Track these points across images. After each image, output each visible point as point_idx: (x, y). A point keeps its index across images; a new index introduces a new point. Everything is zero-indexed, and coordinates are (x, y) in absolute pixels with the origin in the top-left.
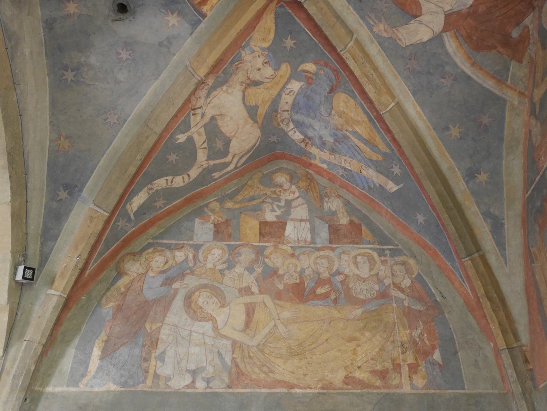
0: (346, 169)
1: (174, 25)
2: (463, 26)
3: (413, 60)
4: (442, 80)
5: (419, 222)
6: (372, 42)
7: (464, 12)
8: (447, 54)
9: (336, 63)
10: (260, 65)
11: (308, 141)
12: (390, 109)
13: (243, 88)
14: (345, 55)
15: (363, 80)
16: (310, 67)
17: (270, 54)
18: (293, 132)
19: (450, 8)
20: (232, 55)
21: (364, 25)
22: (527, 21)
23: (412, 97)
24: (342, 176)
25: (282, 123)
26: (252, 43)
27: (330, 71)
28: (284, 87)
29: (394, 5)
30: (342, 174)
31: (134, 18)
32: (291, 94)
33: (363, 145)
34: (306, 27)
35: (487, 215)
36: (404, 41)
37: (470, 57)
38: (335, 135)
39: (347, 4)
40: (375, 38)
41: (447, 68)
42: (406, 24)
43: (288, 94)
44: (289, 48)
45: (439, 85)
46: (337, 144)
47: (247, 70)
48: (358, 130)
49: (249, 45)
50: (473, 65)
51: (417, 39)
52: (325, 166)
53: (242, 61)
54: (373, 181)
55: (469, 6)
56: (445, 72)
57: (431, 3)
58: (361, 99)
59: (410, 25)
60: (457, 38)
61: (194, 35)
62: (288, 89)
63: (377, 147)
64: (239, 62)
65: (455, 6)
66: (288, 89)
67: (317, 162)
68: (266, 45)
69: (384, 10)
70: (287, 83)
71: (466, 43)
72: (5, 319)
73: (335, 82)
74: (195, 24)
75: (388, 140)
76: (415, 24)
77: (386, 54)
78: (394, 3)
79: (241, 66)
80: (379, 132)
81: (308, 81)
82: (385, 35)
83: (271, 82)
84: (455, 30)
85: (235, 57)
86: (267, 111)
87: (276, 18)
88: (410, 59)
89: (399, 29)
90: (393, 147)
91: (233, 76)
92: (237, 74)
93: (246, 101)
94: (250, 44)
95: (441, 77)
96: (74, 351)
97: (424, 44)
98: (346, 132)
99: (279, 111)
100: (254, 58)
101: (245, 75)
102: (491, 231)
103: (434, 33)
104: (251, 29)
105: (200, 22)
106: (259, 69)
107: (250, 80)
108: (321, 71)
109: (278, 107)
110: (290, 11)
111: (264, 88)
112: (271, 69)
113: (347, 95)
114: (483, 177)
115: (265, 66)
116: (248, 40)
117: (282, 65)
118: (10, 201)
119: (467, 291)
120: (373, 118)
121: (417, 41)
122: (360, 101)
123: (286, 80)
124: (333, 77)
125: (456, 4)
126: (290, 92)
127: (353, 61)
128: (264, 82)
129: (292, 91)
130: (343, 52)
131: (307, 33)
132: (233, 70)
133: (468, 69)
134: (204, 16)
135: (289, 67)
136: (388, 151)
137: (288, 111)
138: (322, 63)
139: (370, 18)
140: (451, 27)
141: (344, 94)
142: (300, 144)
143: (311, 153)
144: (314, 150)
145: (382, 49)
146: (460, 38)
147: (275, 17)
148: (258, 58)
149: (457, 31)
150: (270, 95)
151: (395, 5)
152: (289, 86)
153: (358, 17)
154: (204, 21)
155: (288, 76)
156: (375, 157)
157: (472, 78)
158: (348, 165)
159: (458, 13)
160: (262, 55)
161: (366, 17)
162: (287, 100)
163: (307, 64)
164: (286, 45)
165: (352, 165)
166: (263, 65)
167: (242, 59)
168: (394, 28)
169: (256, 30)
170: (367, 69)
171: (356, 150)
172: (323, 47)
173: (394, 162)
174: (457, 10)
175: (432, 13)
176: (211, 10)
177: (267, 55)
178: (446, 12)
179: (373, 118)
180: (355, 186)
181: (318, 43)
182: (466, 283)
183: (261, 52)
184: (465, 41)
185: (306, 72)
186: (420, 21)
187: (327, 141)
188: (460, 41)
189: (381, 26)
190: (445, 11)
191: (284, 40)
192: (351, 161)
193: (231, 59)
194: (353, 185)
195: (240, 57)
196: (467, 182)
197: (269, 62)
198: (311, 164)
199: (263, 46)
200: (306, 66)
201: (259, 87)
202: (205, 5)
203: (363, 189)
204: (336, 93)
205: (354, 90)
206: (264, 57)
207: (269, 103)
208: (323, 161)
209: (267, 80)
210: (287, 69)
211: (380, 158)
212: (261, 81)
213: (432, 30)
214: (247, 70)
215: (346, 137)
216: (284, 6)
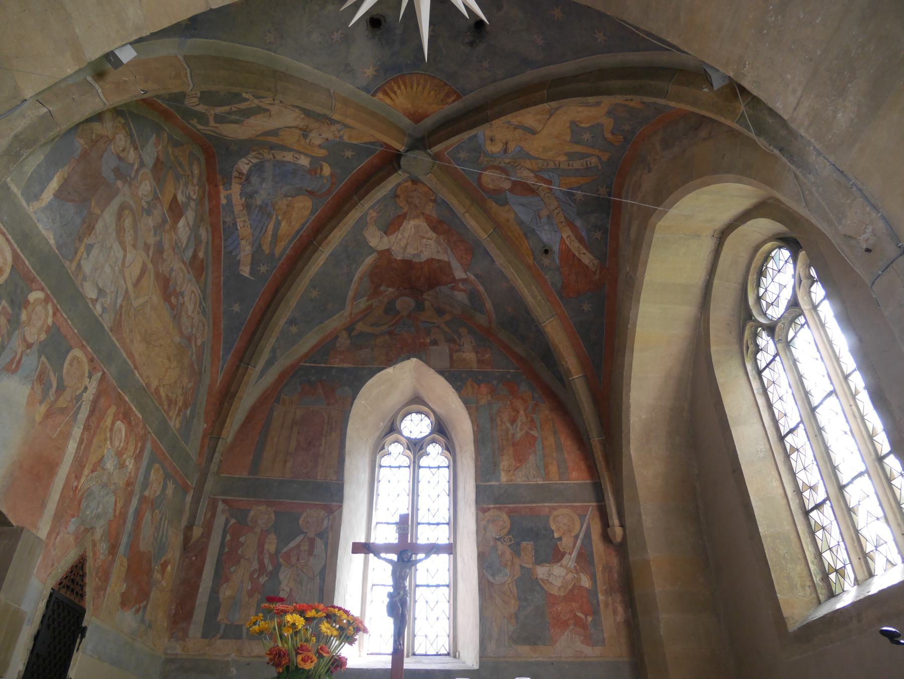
0: (235, 224)
1: (365, 73)
5: (232, 309)
8: (363, 261)
11: (244, 177)
16: (327, 170)
18: (248, 162)
22: (390, 290)
24: (225, 222)
25: (256, 154)
28: (301, 153)
30: (227, 221)
31: (370, 39)
32: (295, 159)
33: (271, 233)
35: (274, 351)
38: (267, 205)
42: (378, 229)
43: (293, 156)
44: (343, 154)
46: (258, 209)
48: (283, 224)
52: (224, 201)
54: (240, 253)
61: (356, 90)
62: (300, 156)
63: (276, 245)
66: (300, 156)
67: (223, 194)
70: (306, 155)
72: (69, 70)
74: (367, 90)
75: (287, 252)
80: (290, 242)
82: (369, 218)
89: (374, 226)
90: (283, 259)
96: (43, 157)
98: (275, 214)
99: (272, 151)
102: (266, 361)
105: (368, 91)
113: (311, 207)
114: (294, 329)
118: (211, 9)
119: (217, 380)
120: (301, 233)
126: (296, 158)
129: (298, 159)
133: (356, 278)
134: (374, 95)
135: (324, 155)
136: (277, 256)
137: (274, 158)
139: (379, 206)
141: (311, 203)
142: (234, 170)
143: (231, 185)
144: (236, 188)
148: (332, 134)
152: (302, 157)
153: (379, 198)
154: (369, 96)
155: (314, 155)
156: (266, 248)
158: (241, 225)
162: (288, 157)
163: (329, 168)
165: (244, 227)
171: (262, 229)
173: (269, 264)
176: (379, 99)
179: (301, 233)
180: (223, 238)
182: (222, 374)
183: (339, 135)
187: (256, 199)
189: (374, 214)
192: (247, 227)
194: (222, 236)
196: (286, 323)
198: (216, 186)
202: (383, 94)
203: (225, 247)
205: (319, 211)
208: (229, 198)
211: (267, 252)
215: (269, 216)
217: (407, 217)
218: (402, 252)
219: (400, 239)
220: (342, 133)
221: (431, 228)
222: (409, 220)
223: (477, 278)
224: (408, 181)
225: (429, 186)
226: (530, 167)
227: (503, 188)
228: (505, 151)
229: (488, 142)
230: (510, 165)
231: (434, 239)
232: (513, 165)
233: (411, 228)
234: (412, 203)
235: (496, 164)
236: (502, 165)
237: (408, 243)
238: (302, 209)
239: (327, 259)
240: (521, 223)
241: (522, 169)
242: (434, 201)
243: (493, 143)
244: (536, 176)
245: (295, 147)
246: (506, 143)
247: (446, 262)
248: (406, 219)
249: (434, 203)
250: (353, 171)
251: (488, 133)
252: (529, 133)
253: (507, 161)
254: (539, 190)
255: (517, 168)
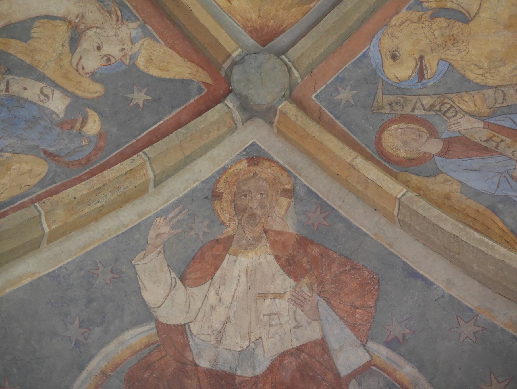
2: (166, 355)
3: (111, 275)
4: (77, 322)
6: (140, 216)
7: (188, 354)
8: (122, 330)
9: (102, 162)
10: (106, 50)
12: (40, 222)
13: (72, 17)
14: (138, 159)
15: (96, 182)
17: (124, 68)
19: (194, 332)
20: (135, 8)
21: (168, 204)
23: (47, 272)
26: (147, 41)
27: (86, 153)
28: (56, 86)
29: (202, 245)
32: (42, 97)
34: (164, 122)
36: (143, 262)
37: (116, 368)
39: (203, 179)
40: (147, 220)
41: (97, 331)
43: (42, 92)
44: (129, 96)
45: (69, 317)
47: (103, 29)
49: (145, 36)
50: (103, 373)
51: (146, 283)
53: (120, 21)
55: (197, 361)
56: (92, 328)
57: (203, 302)
58: (39, 193)
59: (168, 272)
60: (146, 347)
64: (120, 17)
65: (197, 340)
68: (141, 62)
69: (193, 233)
70: (65, 91)
71: (139, 361)
73: (67, 159)
76: (169, 280)
77: (120, 234)
78: (204, 245)
79: (112, 18)
81: (66, 123)
82: (152, 234)
83: (72, 65)
84: (159, 343)
85: (130, 11)
86: (12, 57)
87: (182, 81)
88: (112, 271)
89: (161, 256)
91: (98, 5)
92: (100, 11)
93: (45, 20)
94: (146, 39)
95: (83, 321)
97: (138, 292)
100: (122, 42)
101: (95, 24)
103: (155, 308)
104: (170, 42)
106: (99, 48)
107: (84, 32)
108: (86, 141)
109: (16, 75)
110: (192, 101)
111: (61, 54)
112: (96, 67)
115: (102, 58)
116: (154, 36)
117: (100, 85)
121: (142, 282)
122: (36, 192)
123: (71, 90)
124: (76, 158)
125: (201, 340)
126: (46, 96)
127: (129, 169)
128: (72, 55)
129: (48, 98)
130: (143, 156)
131: (154, 124)
132: (108, 5)
135: (96, 95)
137: (7, 90)
138: (102, 143)
140: (163, 336)
145: (129, 230)
146: (147, 350)
147: (184, 80)
148: (120, 47)
149: (158, 346)
150: (46, 64)
151: (201, 247)
152: (57, 94)
153: (181, 195)
155: (79, 93)
157: (80, 373)
159: (186, 346)
160: (125, 55)
161: (181, 206)
163: (98, 122)
164: (135, 92)
166: (106, 56)
167: (125, 22)
168: (163, 248)
169: (168, 49)
170: (109, 194)
172: (131, 146)
174: (190, 344)
175: (188, 303)
177: (124, 63)
178: (189, 326)
181: (137, 139)
183: (130, 53)
184: (143, 359)
185: (83, 121)
186: (174, 287)
188: (142, 352)
189: (165, 229)
190: (190, 324)
191: (145, 90)
193: (129, 5)
195: (128, 19)
197: (110, 65)
199: (139, 58)
200: (95, 121)
201: (67, 44)
204: (46, 160)
205: (55, 185)
206: (119, 58)
207: (28, 60)
209: (75, 60)
210: (93, 93)
212: (76, 49)
213: (160, 306)
214: (103, 29)
216: (200, 94)
217: (233, 248)
218: (213, 343)
219: (212, 308)
220: (137, 46)
221: (283, 267)
222: (236, 254)
223: (394, 350)
224: (240, 161)
225: (281, 162)
226: (472, 109)
227: (425, 153)
228: (421, 74)
229: (389, 62)
230: (432, 113)
231: (287, 296)
232: (440, 111)
233: (239, 276)
234: (245, 210)
235: (407, 110)
236: (419, 112)
237: (227, 320)
238: (24, 174)
239: (40, 278)
240: (477, 194)
241: (459, 115)
242: (289, 193)
243: (398, 61)
244: (488, 126)
245: (48, 73)
246: (422, 58)
247: (315, 343)
248: (230, 251)
249: (290, 197)
250: (141, 134)
251: (388, 44)
252: (458, 20)
253: (427, 101)
254: (499, 147)
255: (448, 115)
